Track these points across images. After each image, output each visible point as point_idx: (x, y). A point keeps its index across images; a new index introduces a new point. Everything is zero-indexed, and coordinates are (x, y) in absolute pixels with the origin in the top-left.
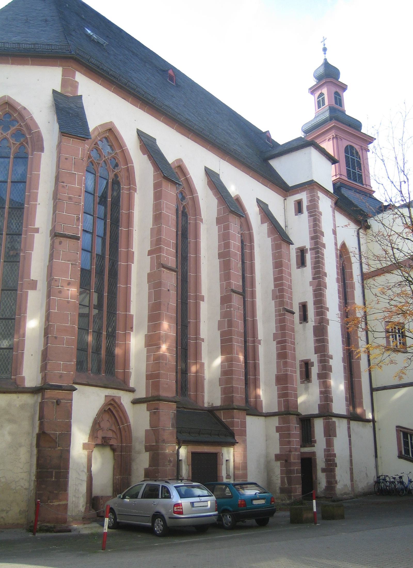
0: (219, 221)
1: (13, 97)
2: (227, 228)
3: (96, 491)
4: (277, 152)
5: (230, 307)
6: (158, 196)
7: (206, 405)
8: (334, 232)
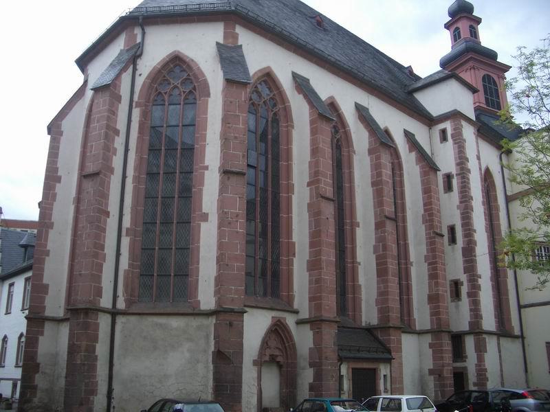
0: (371, 152)
1: (182, 51)
2: (378, 158)
3: (266, 403)
4: (420, 85)
5: (385, 232)
6: (314, 132)
7: (364, 324)
8: (478, 158)
